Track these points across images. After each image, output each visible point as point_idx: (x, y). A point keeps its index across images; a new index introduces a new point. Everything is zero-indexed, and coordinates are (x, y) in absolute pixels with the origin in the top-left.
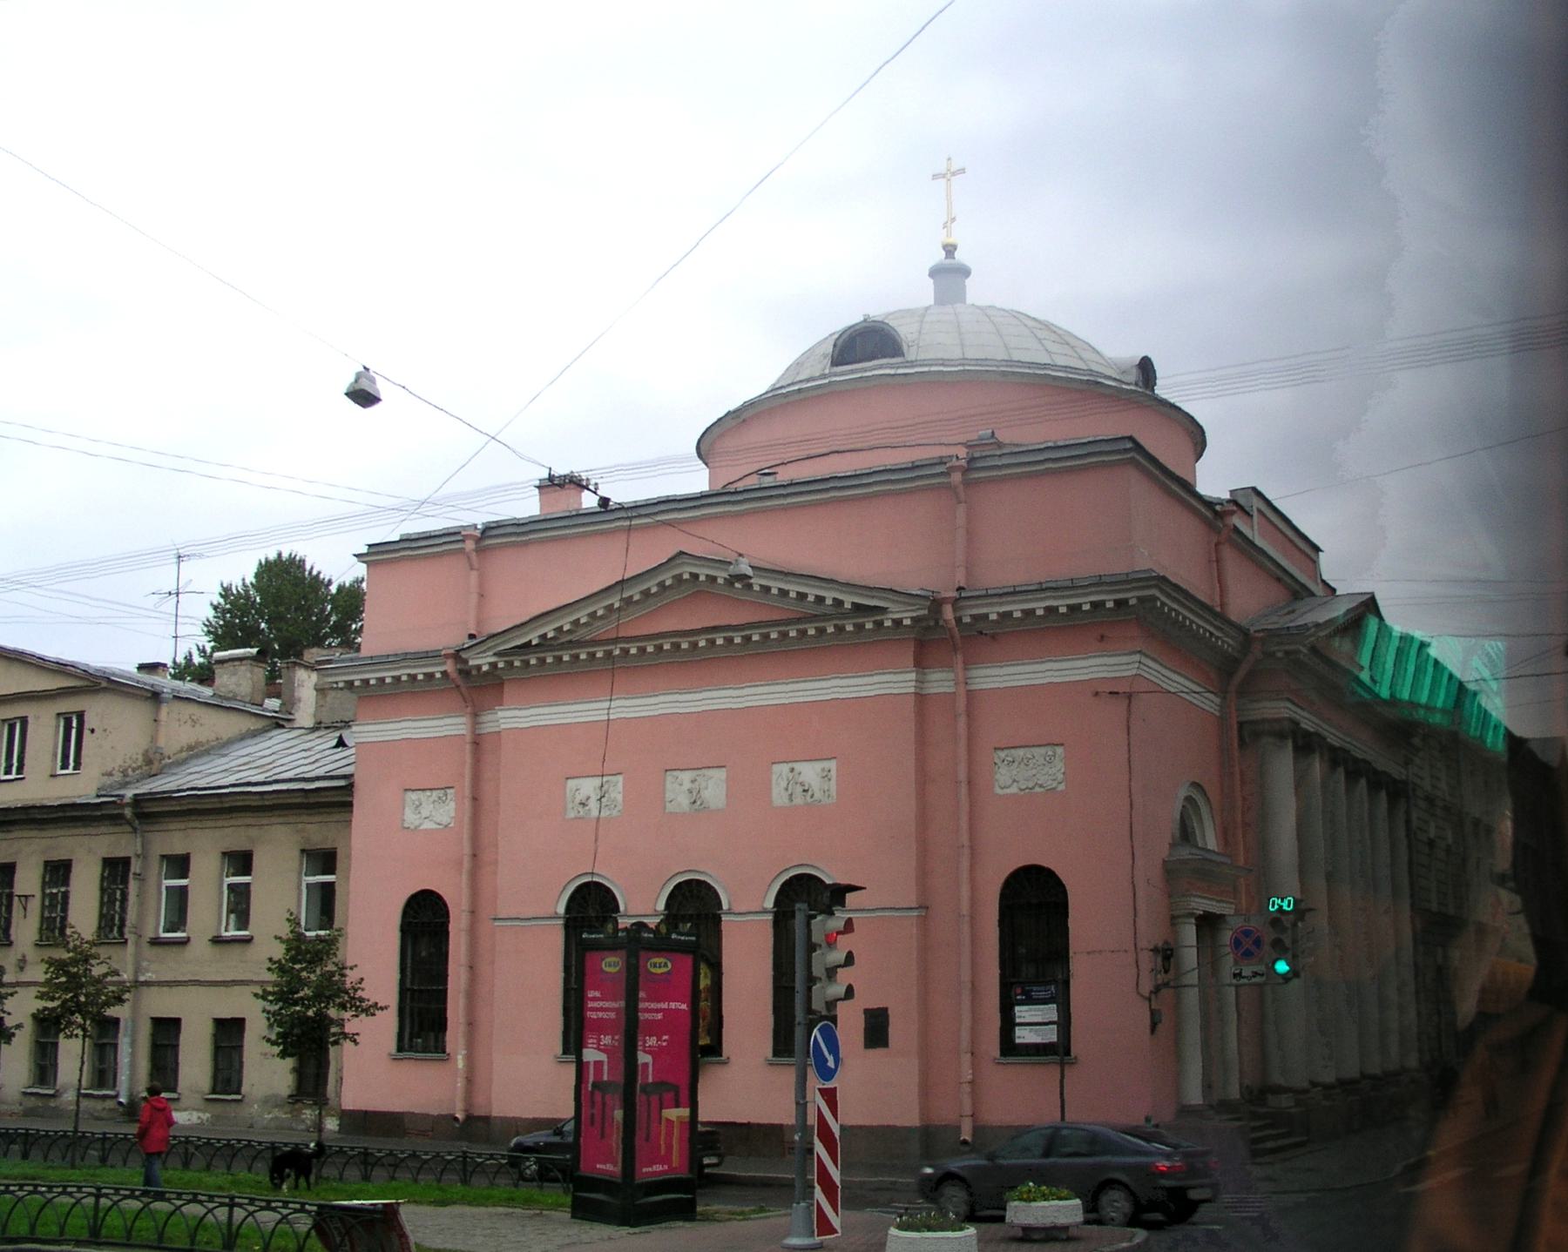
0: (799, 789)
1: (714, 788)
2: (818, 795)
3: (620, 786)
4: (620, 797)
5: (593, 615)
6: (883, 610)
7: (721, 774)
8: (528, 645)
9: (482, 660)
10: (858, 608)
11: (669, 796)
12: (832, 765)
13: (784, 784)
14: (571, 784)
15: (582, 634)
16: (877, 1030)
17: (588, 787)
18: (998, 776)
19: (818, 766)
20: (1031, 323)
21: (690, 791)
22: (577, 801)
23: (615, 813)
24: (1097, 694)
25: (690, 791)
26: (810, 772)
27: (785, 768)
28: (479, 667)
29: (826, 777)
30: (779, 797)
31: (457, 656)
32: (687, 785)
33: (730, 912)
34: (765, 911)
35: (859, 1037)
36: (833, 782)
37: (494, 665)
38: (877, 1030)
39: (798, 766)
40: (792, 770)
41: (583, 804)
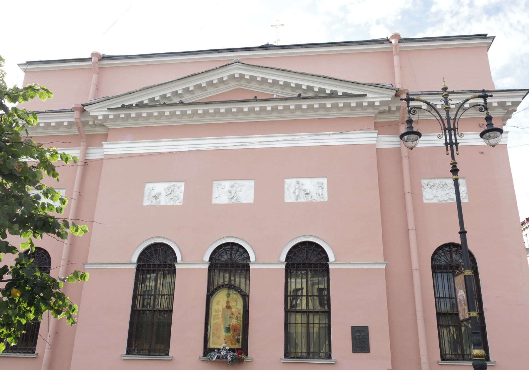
0: (303, 193)
3: (182, 188)
4: (181, 196)
5: (221, 81)
9: (98, 112)
10: (346, 95)
13: (292, 190)
14: (149, 186)
15: (187, 99)
16: (361, 340)
17: (160, 188)
18: (424, 193)
19: (315, 181)
20: (434, 275)
21: (230, 192)
22: (153, 194)
23: (177, 203)
24: (444, 79)
25: (230, 192)
28: (96, 117)
29: (321, 186)
31: (83, 110)
33: (256, 262)
34: (282, 263)
35: (348, 343)
36: (241, 337)
37: (106, 117)
38: (361, 340)
40: (298, 183)
41: (156, 197)
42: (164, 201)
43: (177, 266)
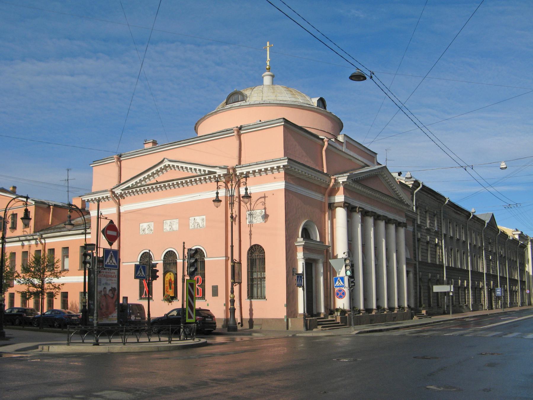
0: (196, 224)
1: (176, 227)
2: (201, 226)
6: (215, 173)
7: (177, 221)
8: (129, 187)
10: (210, 173)
11: (164, 227)
12: (204, 217)
16: (215, 292)
17: (144, 225)
26: (199, 219)
27: (193, 218)
29: (203, 220)
30: (191, 226)
32: (169, 224)
39: (196, 218)
42: (147, 232)
43: (205, 259)
